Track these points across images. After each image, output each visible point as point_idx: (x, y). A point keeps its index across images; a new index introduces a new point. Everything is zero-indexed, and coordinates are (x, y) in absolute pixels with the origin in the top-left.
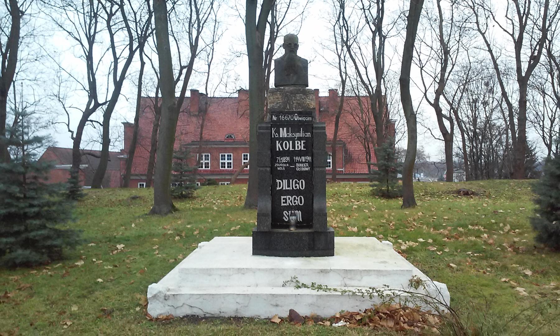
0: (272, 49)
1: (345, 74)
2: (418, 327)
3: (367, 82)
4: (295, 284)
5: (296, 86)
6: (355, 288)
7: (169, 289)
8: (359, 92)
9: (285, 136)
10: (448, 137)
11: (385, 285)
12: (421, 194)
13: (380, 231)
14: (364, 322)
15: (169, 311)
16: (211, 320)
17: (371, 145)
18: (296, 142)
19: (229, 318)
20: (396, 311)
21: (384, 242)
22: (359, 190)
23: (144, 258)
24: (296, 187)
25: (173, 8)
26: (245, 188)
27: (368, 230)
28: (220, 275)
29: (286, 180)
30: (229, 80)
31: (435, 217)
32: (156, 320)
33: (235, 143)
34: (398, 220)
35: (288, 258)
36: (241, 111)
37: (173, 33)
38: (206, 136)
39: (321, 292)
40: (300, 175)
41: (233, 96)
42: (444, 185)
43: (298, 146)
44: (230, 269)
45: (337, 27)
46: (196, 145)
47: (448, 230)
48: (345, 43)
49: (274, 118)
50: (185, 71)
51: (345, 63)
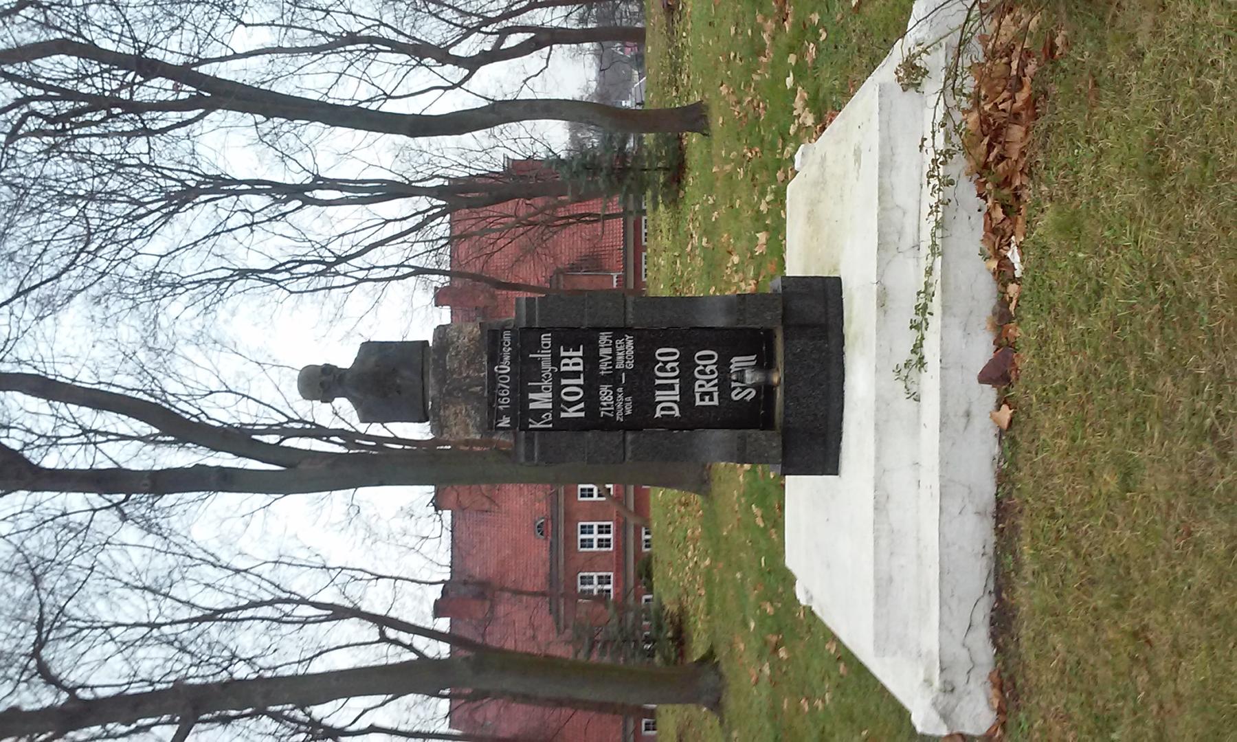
0: (341, 433)
1: (401, 269)
2: (1022, 66)
3: (420, 218)
4: (915, 370)
5: (425, 369)
6: (923, 222)
7: (925, 681)
8: (441, 238)
9: (550, 395)
10: (544, 37)
11: (921, 147)
12: (674, 94)
13: (765, 179)
14: (1011, 201)
15: (980, 682)
16: (1003, 576)
17: (562, 212)
18: (563, 369)
19: (999, 532)
20: (984, 120)
21: (797, 166)
22: (664, 234)
23: (833, 735)
24: (673, 370)
25: (249, 661)
26: (658, 495)
27: (763, 207)
28: (892, 554)
29: (658, 393)
30: (413, 531)
31: (732, 54)
32: (1005, 713)
33: (555, 517)
34: (739, 140)
35: (845, 388)
36: (483, 504)
37: (304, 660)
38: (539, 583)
39: (936, 306)
40: (645, 360)
41: (450, 522)
42: (653, 44)
43: (574, 364)
44: (876, 530)
45: (293, 286)
46: (558, 605)
47: (765, 20)
48: (329, 267)
49: (505, 422)
50: (391, 633)
51: (374, 267)
